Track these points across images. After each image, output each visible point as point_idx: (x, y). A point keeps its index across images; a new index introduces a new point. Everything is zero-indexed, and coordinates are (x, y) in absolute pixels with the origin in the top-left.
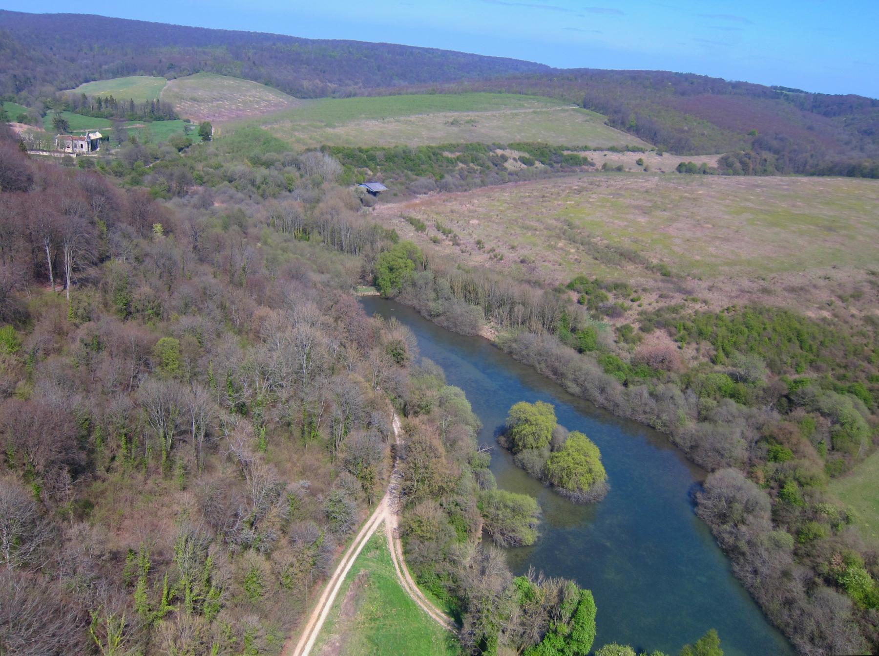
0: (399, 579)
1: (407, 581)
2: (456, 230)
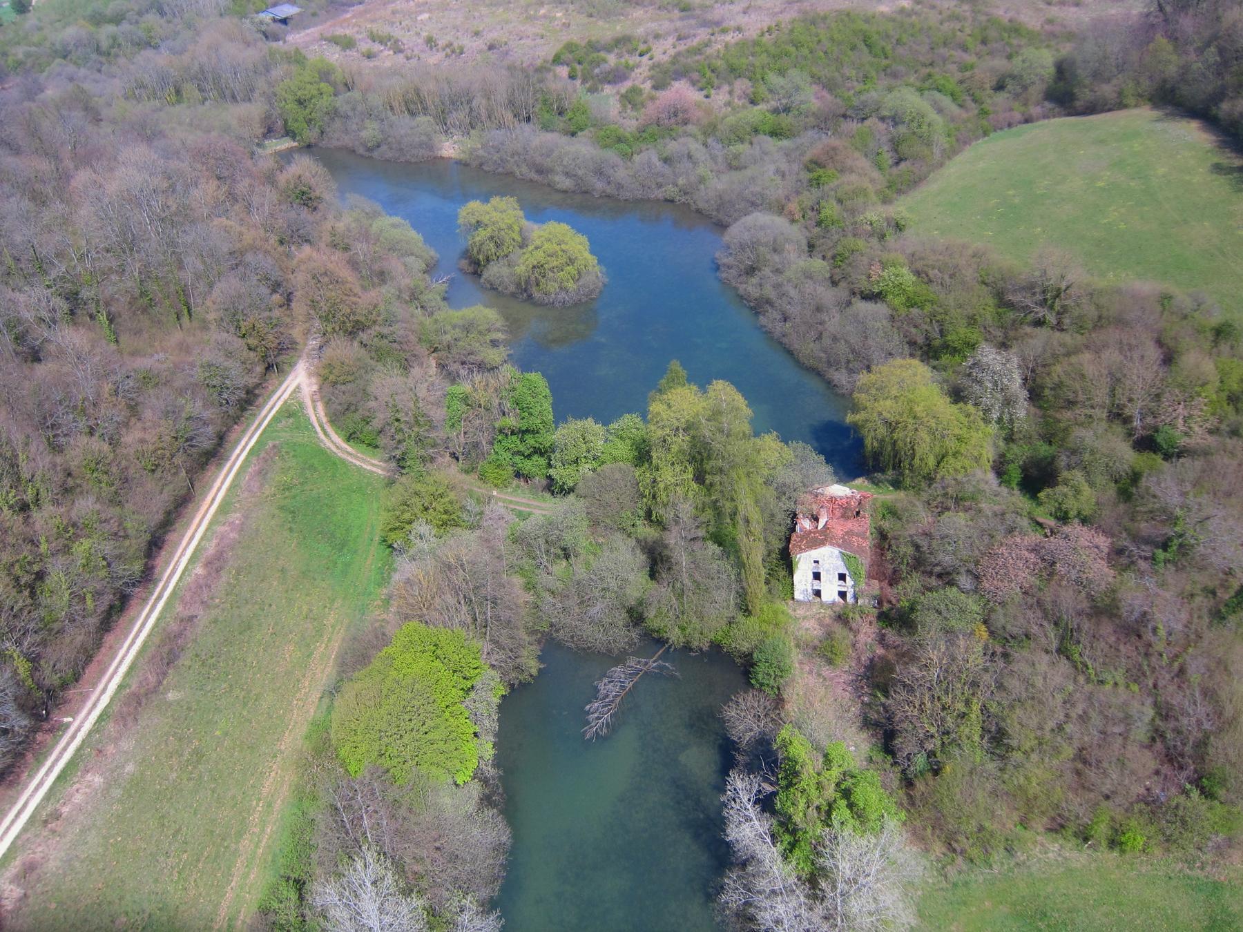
0: (322, 441)
1: (334, 441)
2: (397, 33)
